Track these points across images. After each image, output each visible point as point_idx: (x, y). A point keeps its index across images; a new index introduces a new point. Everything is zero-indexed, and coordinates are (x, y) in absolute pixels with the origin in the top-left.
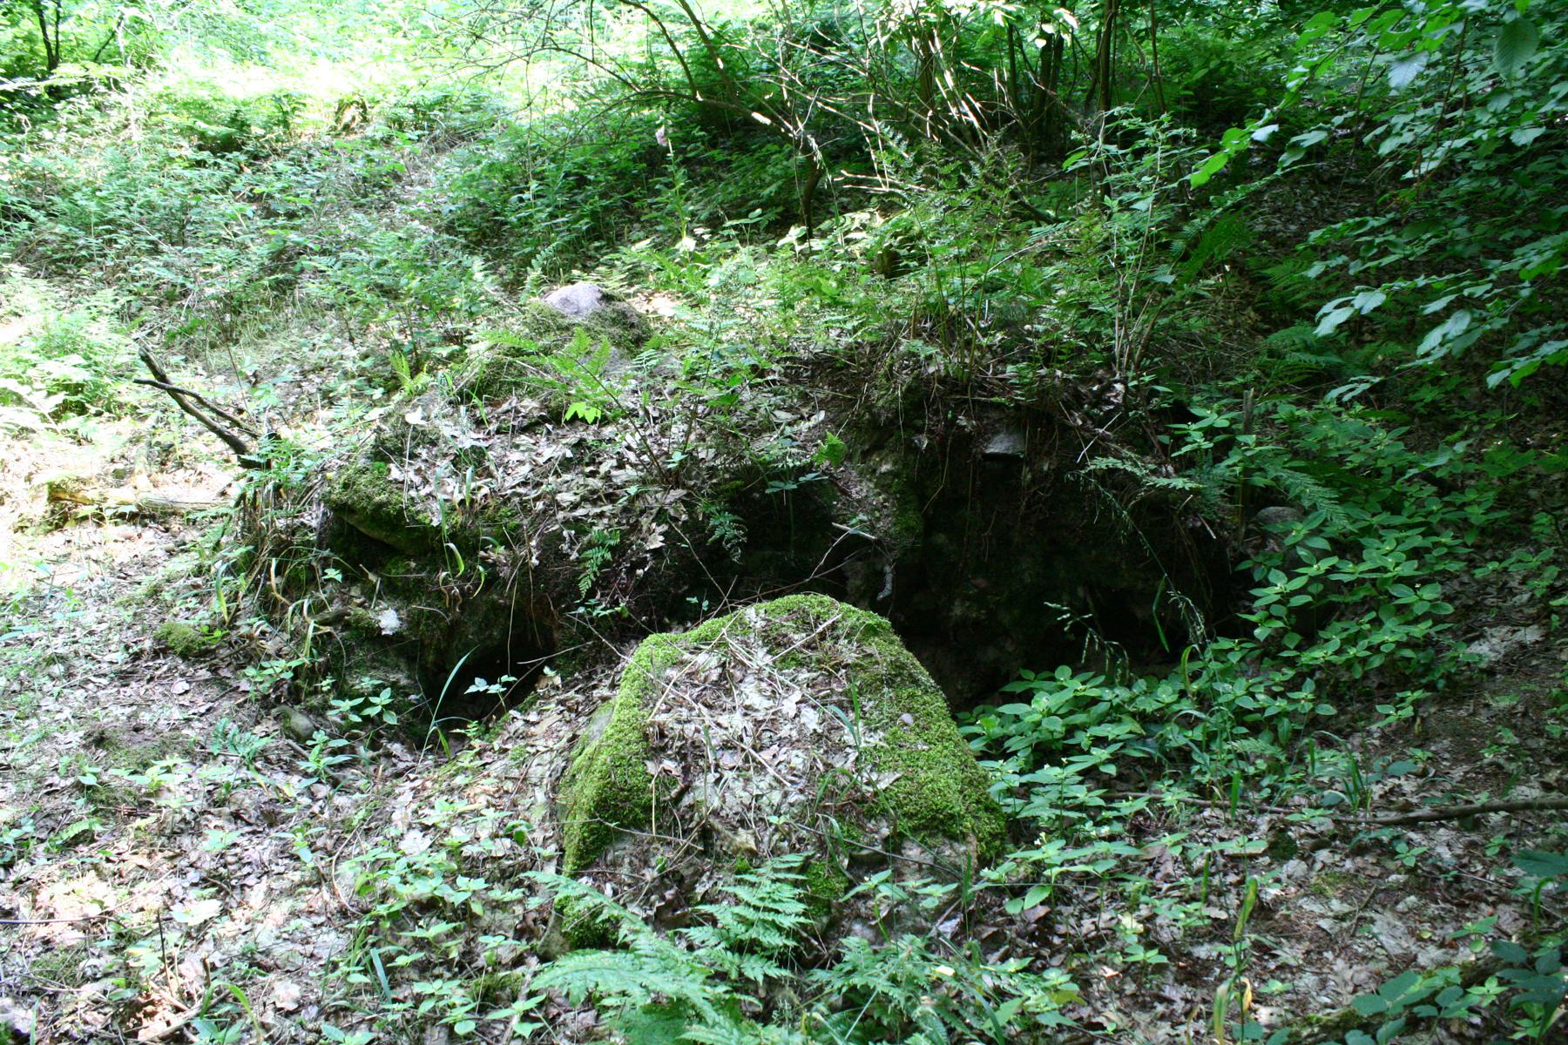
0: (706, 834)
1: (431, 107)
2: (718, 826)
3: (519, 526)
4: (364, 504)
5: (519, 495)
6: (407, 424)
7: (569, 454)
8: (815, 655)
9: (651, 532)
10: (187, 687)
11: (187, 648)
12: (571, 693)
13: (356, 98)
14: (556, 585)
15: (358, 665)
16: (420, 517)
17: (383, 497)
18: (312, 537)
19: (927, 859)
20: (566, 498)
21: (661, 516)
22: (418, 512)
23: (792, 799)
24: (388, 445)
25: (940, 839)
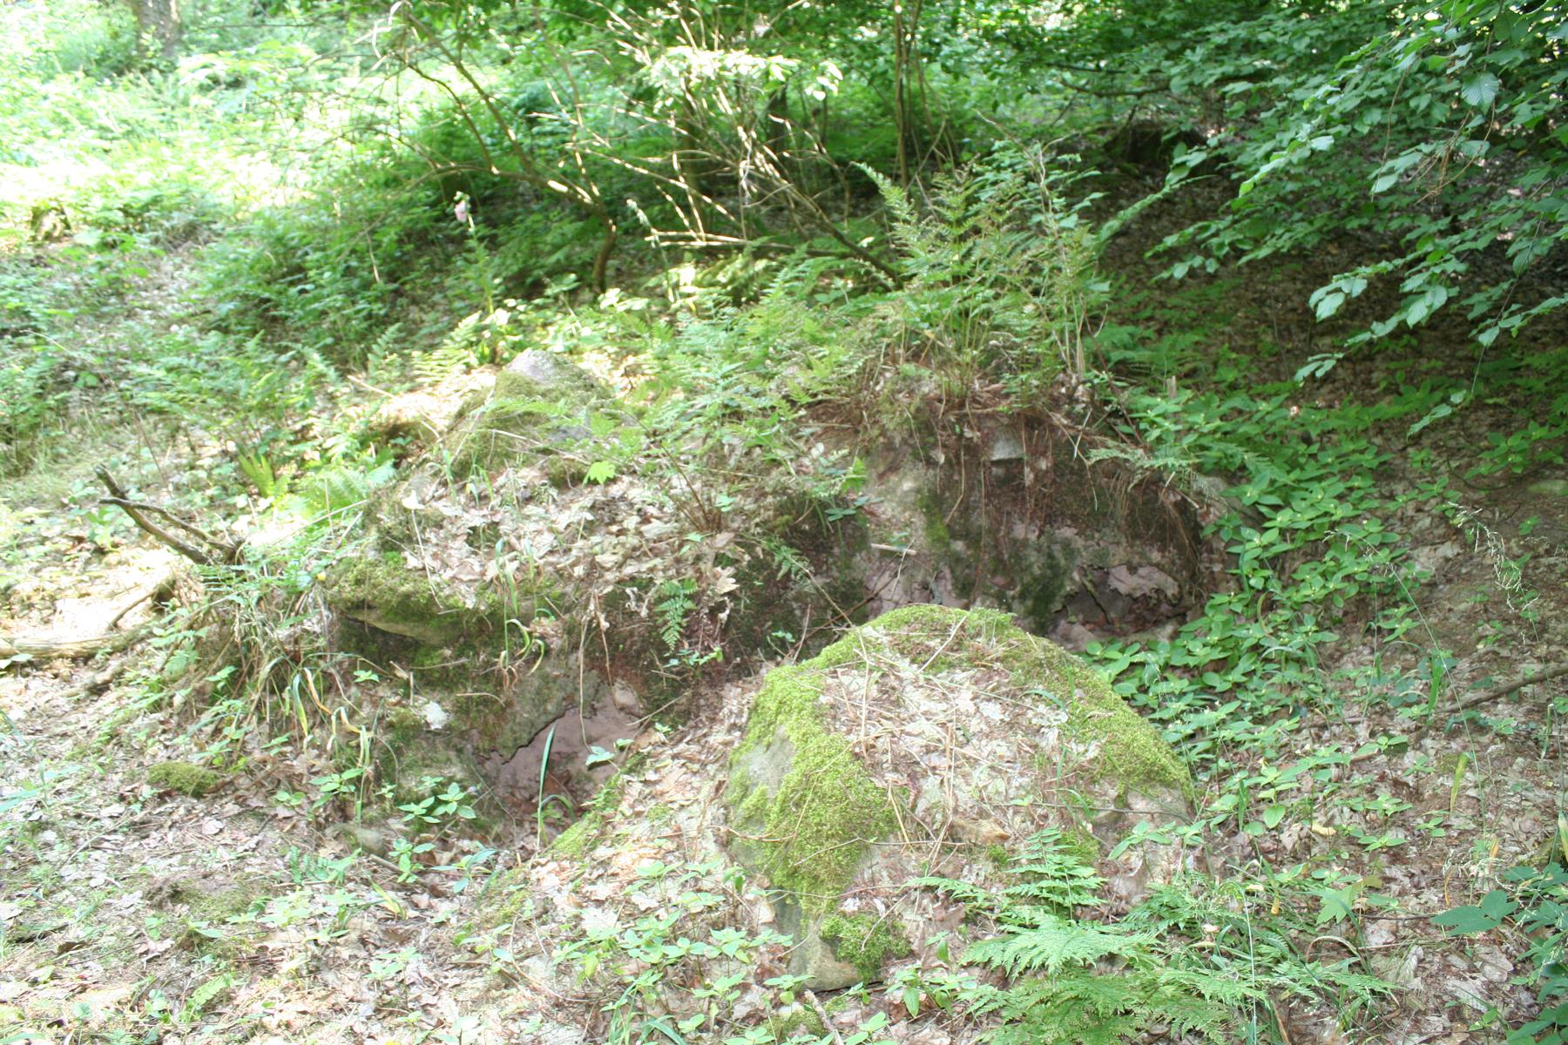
0: (953, 833)
1: (146, 208)
2: (962, 822)
3: (563, 595)
4: (387, 597)
5: (551, 564)
6: (406, 510)
7: (590, 517)
8: (963, 655)
9: (716, 576)
10: (220, 825)
11: (199, 785)
12: (682, 746)
13: (54, 204)
14: (633, 644)
15: (410, 766)
16: (451, 601)
17: (407, 588)
18: (322, 642)
19: (1154, 807)
20: (607, 559)
21: (720, 560)
22: (448, 597)
23: (1015, 783)
24: (395, 533)
25: (1160, 789)
